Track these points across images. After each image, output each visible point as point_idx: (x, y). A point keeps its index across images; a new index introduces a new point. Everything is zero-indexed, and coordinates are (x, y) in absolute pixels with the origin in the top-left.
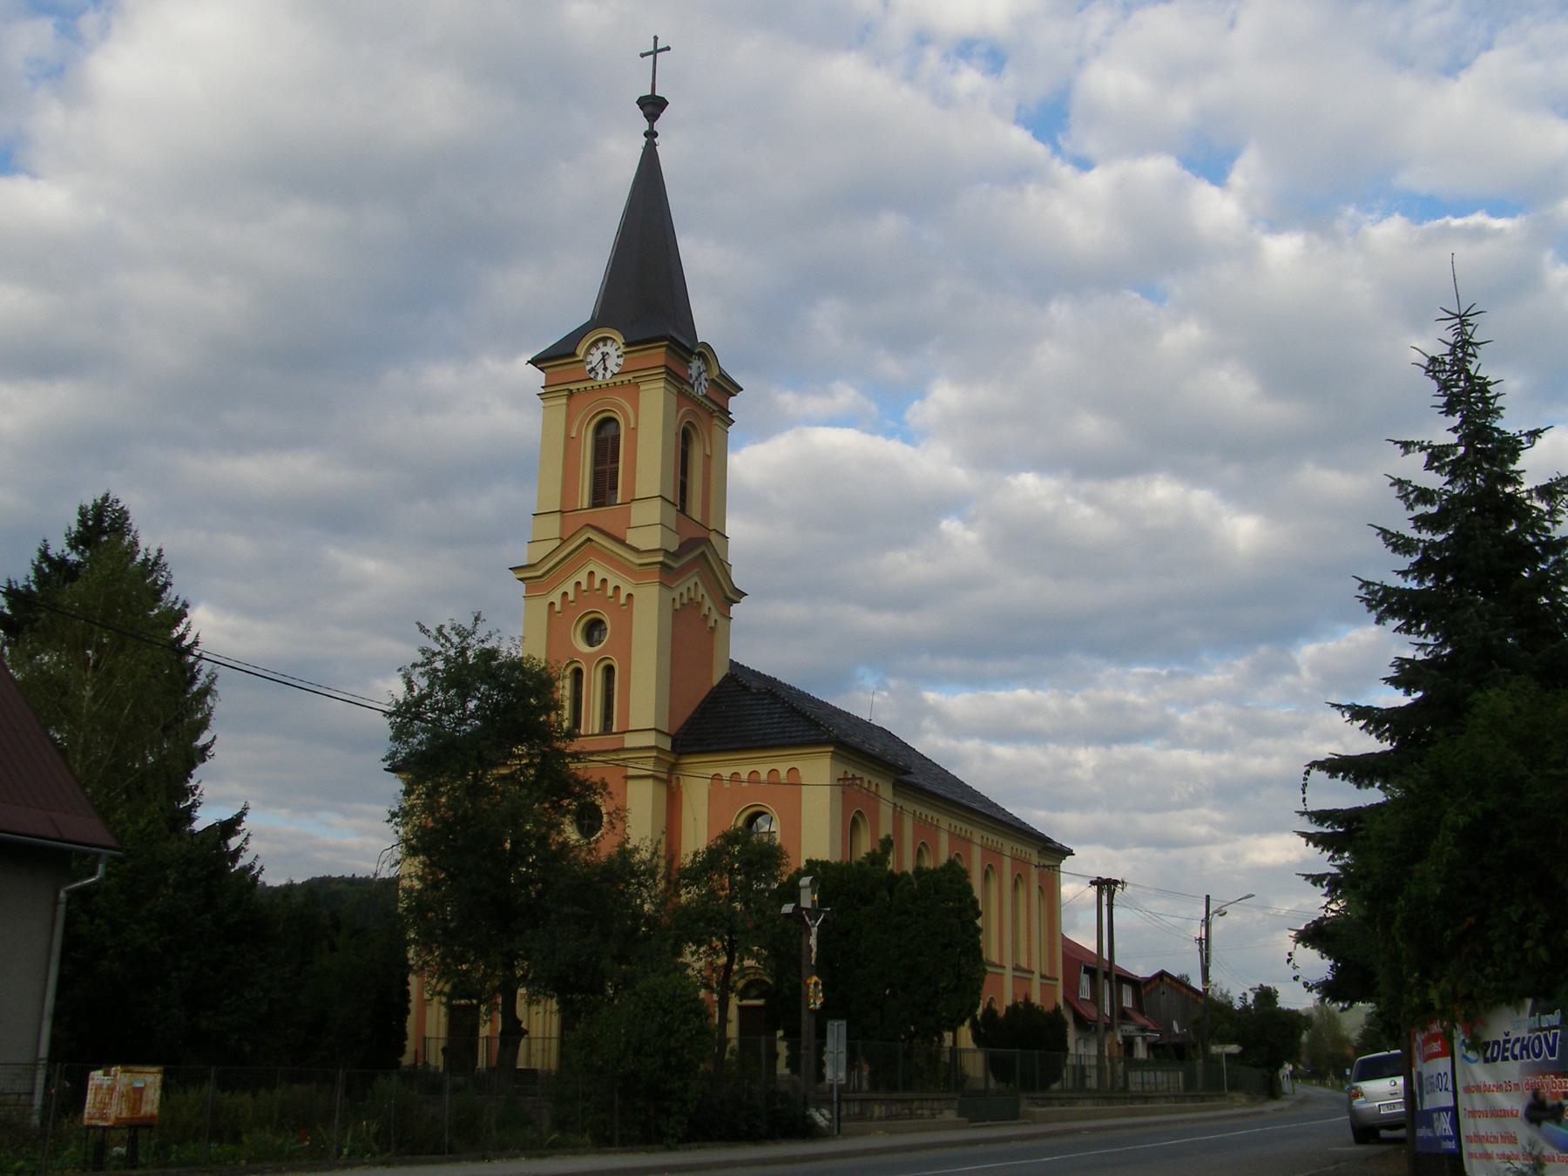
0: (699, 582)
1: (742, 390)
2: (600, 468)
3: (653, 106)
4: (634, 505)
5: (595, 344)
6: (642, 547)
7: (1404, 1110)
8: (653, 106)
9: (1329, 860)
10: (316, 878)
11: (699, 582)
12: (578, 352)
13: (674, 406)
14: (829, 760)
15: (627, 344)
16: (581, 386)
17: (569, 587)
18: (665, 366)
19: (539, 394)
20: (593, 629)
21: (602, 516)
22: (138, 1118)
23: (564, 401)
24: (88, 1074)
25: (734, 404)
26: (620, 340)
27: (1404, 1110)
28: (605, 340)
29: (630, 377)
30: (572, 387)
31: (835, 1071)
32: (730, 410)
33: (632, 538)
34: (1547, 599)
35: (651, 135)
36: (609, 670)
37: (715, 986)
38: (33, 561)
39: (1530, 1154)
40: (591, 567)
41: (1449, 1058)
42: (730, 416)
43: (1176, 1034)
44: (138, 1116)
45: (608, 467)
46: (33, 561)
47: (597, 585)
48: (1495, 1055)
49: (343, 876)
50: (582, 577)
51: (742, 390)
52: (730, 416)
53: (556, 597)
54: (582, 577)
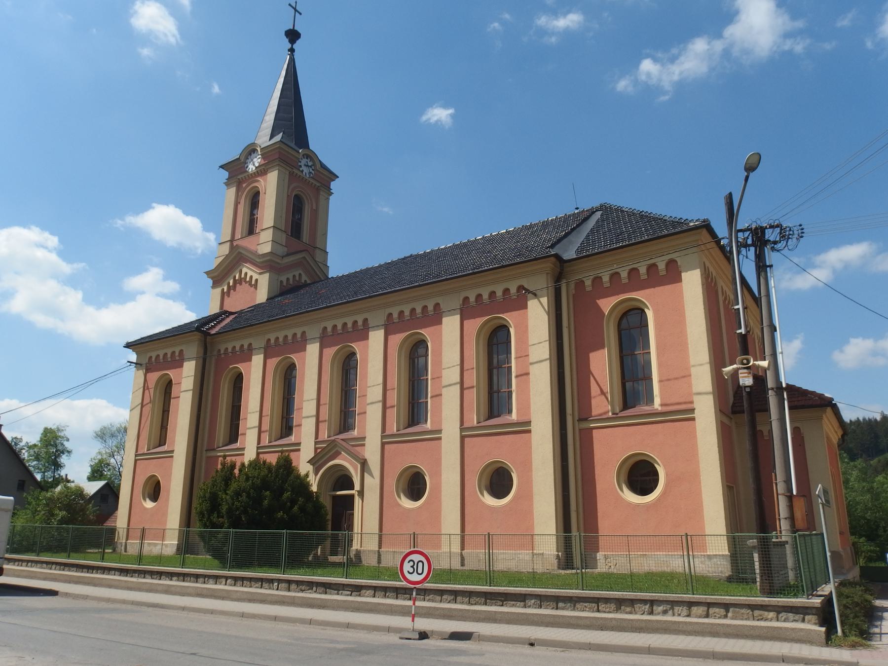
0: (302, 273)
1: (338, 177)
3: (293, 35)
8: (293, 35)
11: (302, 273)
13: (287, 181)
19: (830, 507)
22: (536, 599)
25: (333, 185)
32: (331, 188)
34: (818, 501)
35: (292, 50)
37: (250, 481)
38: (68, 440)
42: (331, 191)
44: (536, 600)
46: (68, 440)
48: (314, 208)
51: (338, 177)
52: (331, 191)
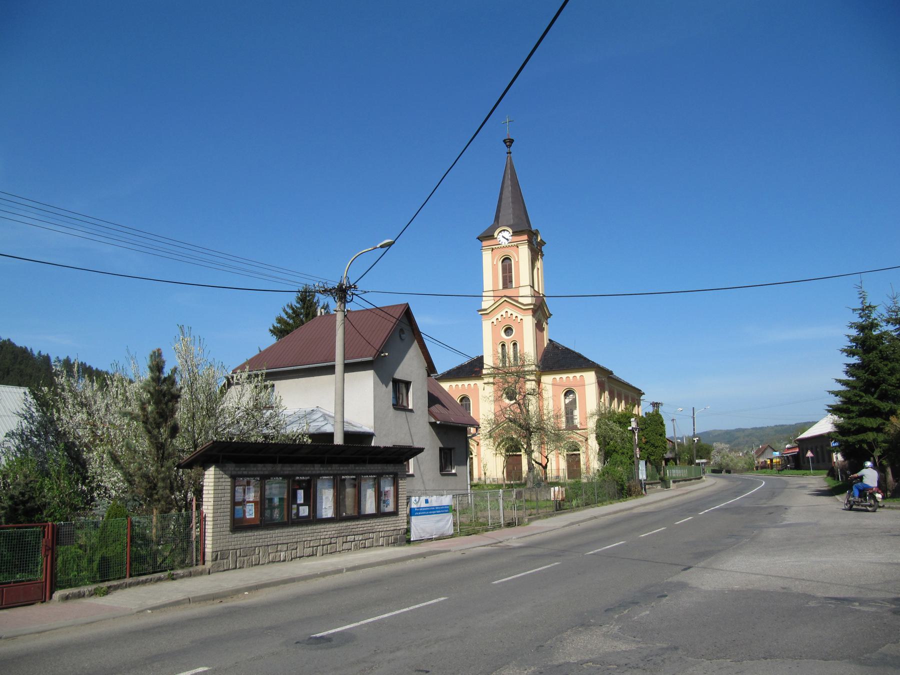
2: (505, 275)
4: (520, 288)
5: (500, 232)
6: (525, 303)
7: (373, 444)
9: (853, 313)
10: (13, 345)
12: (495, 235)
14: (531, 317)
15: (513, 233)
16: (497, 246)
17: (499, 316)
18: (527, 240)
20: (508, 330)
21: (508, 292)
23: (491, 251)
24: (297, 492)
26: (511, 231)
27: (373, 444)
28: (504, 230)
29: (515, 243)
30: (494, 247)
31: (642, 475)
33: (521, 300)
36: (515, 344)
39: (101, 388)
40: (506, 310)
41: (236, 517)
43: (862, 363)
45: (508, 274)
47: (509, 316)
49: (150, 367)
50: (503, 313)
53: (494, 320)
54: (503, 313)
